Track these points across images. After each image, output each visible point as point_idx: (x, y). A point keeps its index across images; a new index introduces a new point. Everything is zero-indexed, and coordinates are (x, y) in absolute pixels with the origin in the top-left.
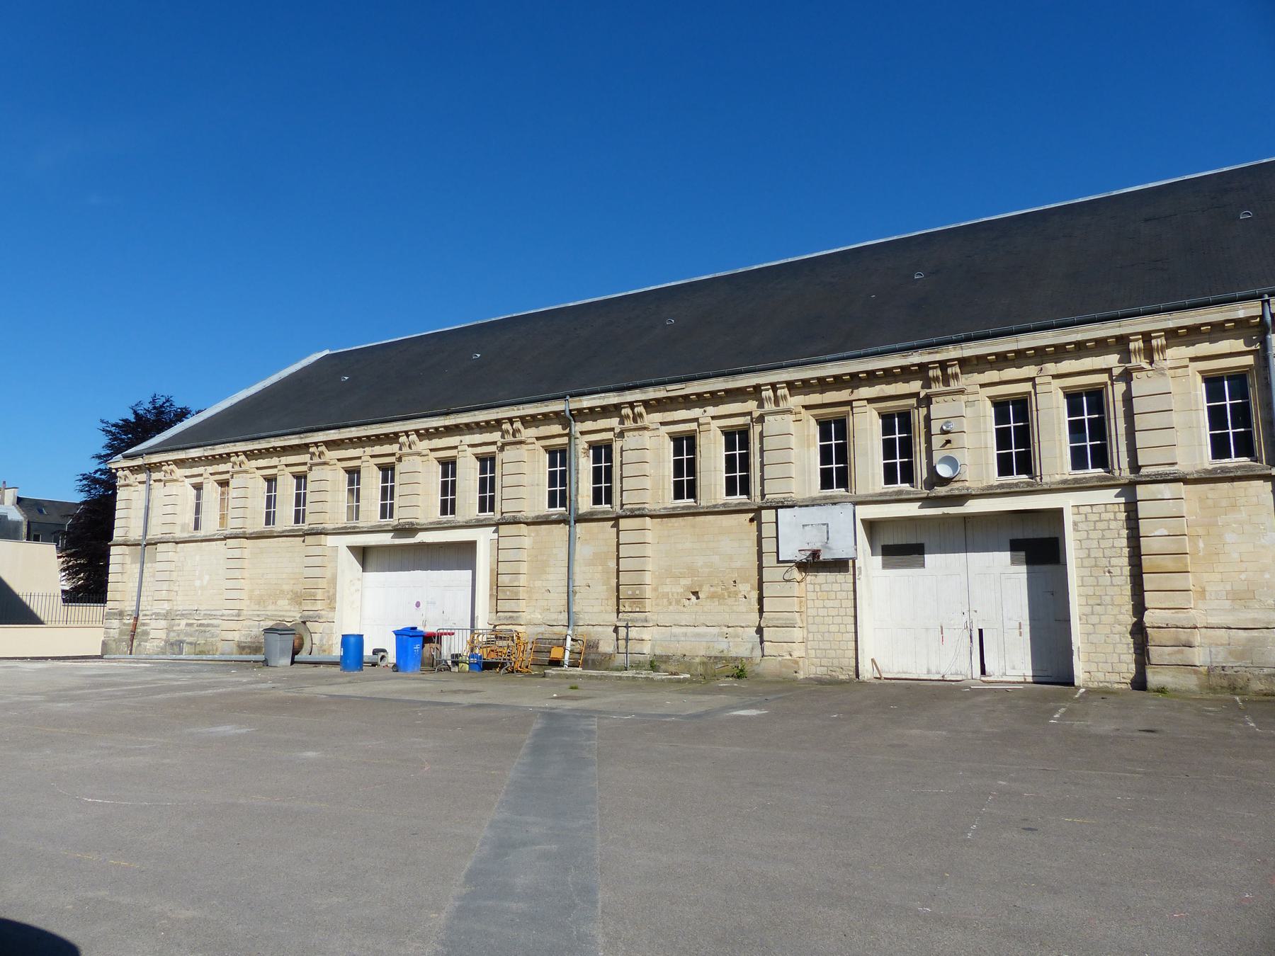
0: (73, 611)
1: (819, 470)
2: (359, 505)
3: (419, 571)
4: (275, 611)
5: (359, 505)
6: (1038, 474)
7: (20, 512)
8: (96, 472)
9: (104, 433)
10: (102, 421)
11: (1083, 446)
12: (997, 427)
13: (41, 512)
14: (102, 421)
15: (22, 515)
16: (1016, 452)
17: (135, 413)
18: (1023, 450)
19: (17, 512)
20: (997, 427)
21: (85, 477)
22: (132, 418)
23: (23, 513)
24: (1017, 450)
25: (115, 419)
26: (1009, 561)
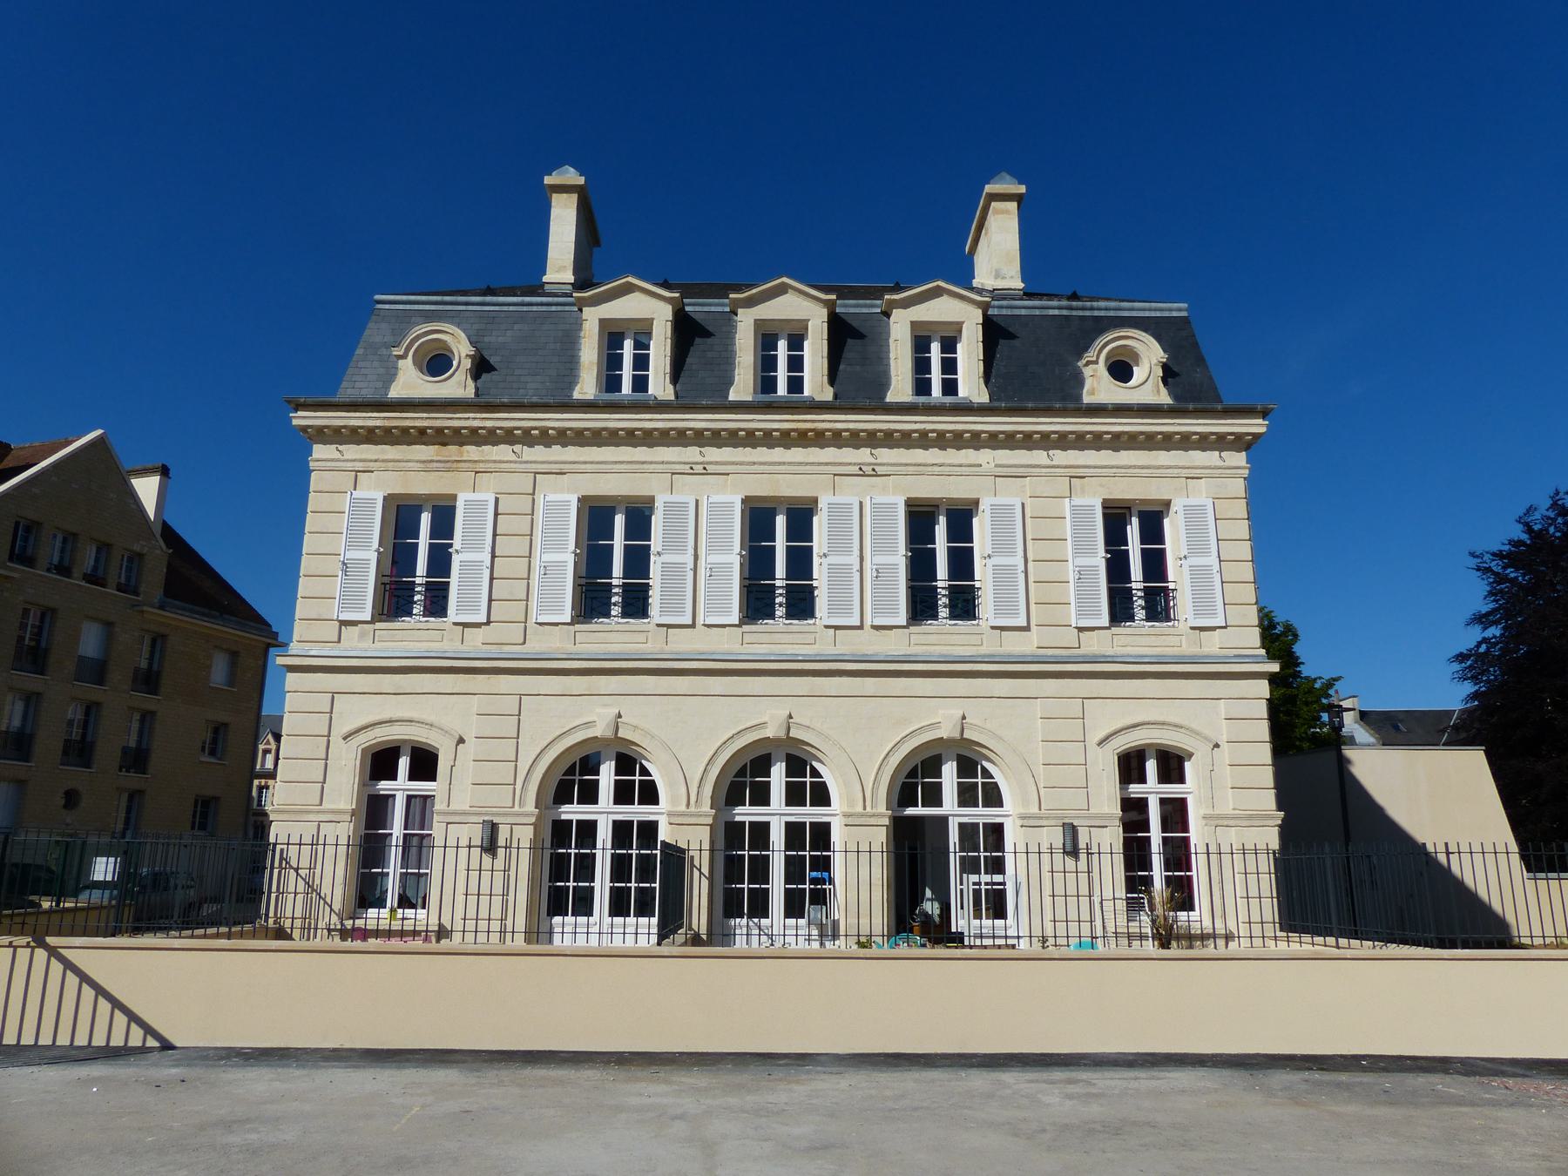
0: (864, 921)
1: (578, 806)
2: (426, 799)
3: (1251, 1052)
4: (1139, 1078)
5: (426, 799)
6: (387, 593)
7: (1367, 731)
8: (1479, 644)
9: (1479, 574)
10: (1473, 555)
11: (571, 779)
12: (648, 352)
13: (1397, 728)
14: (1473, 555)
15: (1372, 735)
16: (811, 777)
17: (1528, 529)
18: (757, 779)
19: (1363, 731)
20: (648, 352)
21: (1461, 657)
22: (1518, 533)
23: (1372, 732)
24: (808, 783)
25: (1498, 542)
26: (599, 249)
